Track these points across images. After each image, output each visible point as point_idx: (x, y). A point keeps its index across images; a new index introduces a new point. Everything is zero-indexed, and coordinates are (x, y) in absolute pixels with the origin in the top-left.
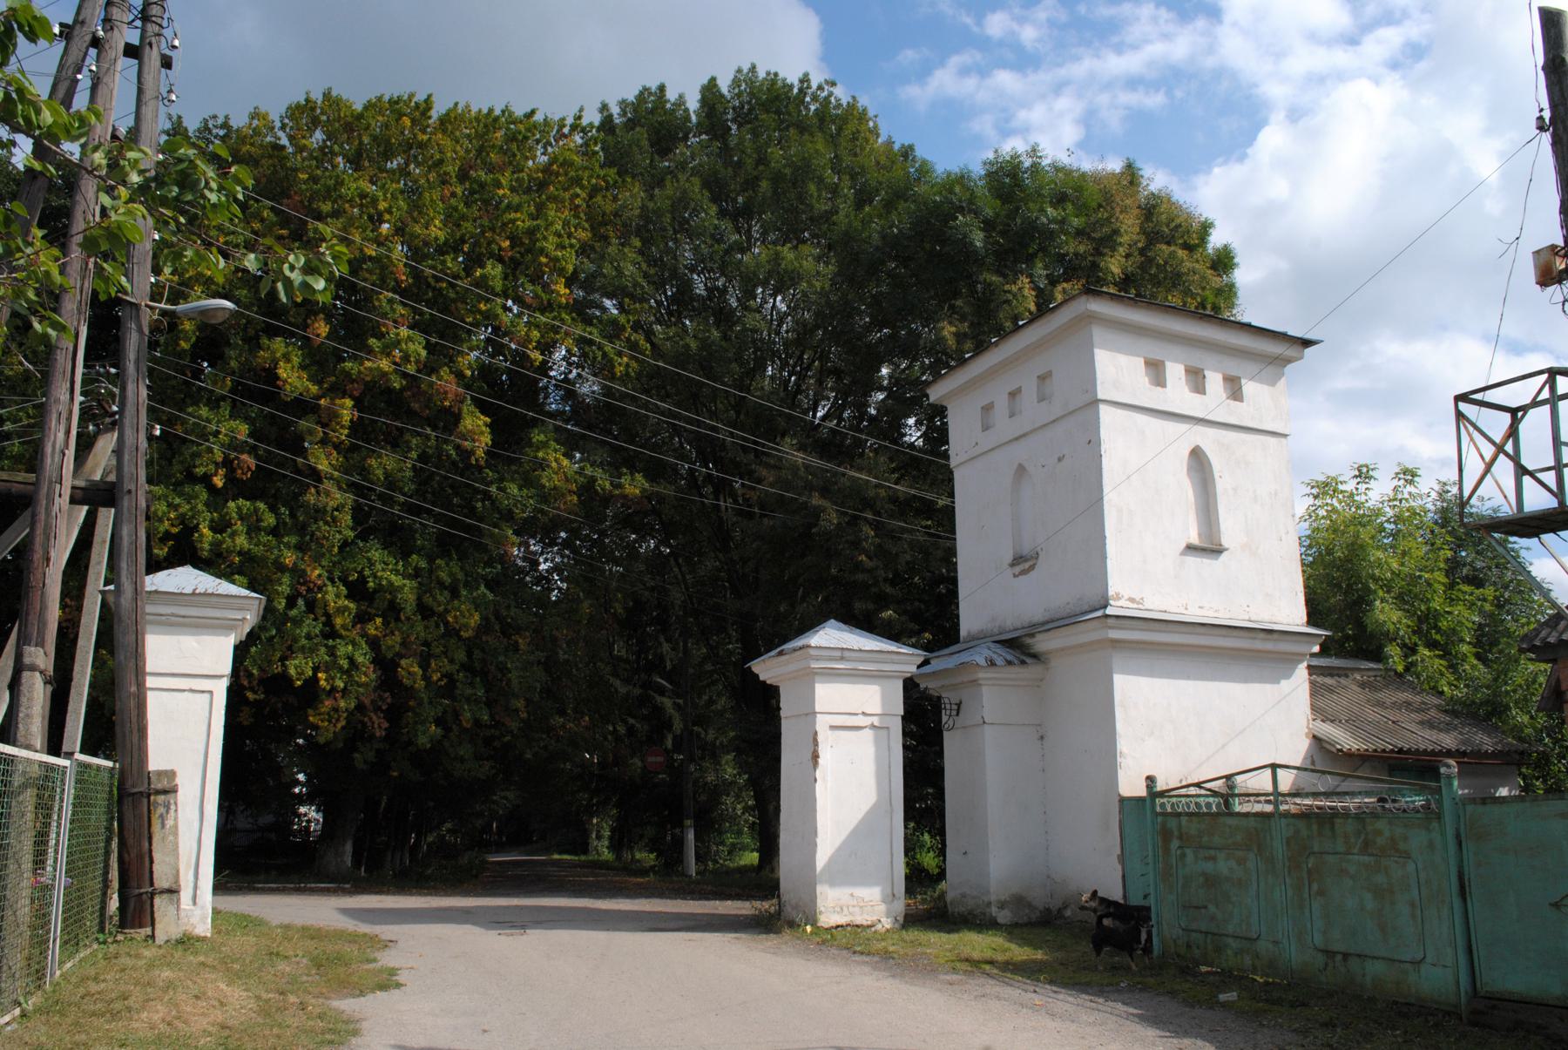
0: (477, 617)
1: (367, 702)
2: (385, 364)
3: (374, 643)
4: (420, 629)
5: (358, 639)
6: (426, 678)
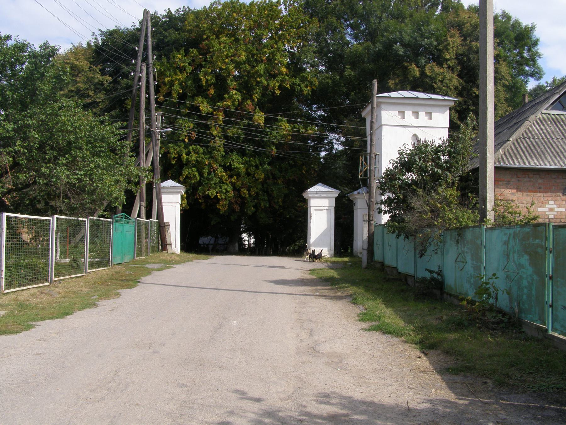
0: (263, 175)
1: (233, 201)
2: (229, 103)
3: (233, 184)
4: (246, 180)
5: (228, 183)
6: (249, 194)
